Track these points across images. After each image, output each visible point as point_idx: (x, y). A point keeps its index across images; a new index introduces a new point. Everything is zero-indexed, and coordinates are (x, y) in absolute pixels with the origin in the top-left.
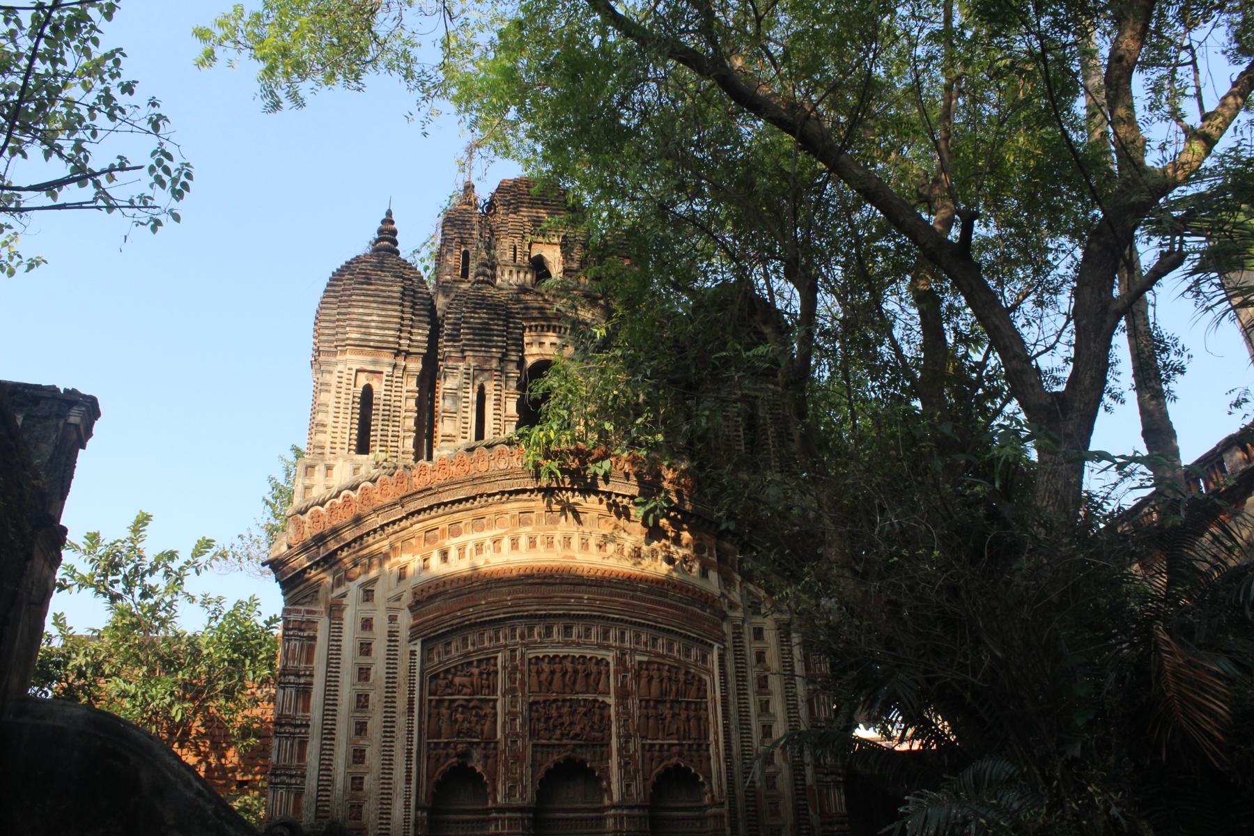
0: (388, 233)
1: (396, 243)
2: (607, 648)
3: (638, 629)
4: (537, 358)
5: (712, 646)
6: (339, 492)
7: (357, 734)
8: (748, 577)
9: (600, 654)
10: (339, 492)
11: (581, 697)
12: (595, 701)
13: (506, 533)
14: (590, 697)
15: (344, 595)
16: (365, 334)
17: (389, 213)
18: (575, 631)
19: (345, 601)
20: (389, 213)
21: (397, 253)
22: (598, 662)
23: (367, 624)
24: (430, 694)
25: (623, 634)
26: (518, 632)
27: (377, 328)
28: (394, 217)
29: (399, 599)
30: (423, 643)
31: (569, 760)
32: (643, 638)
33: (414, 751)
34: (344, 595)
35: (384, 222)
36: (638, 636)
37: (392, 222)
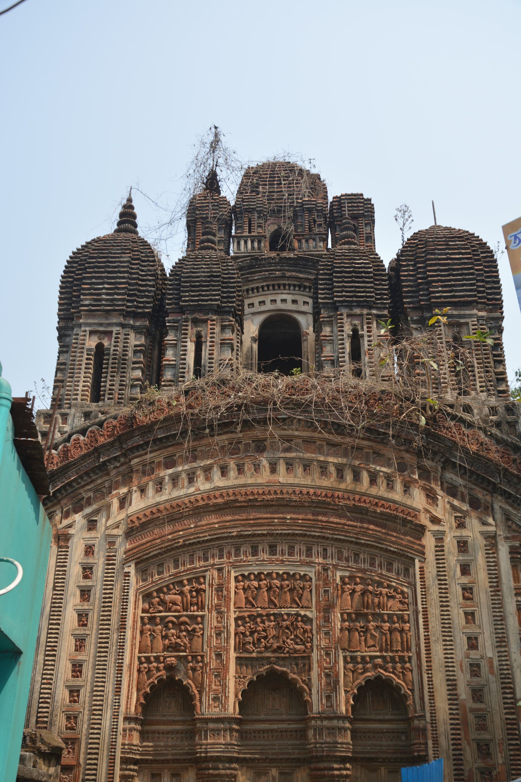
0: (128, 217)
1: (136, 226)
2: (309, 564)
3: (339, 544)
4: (269, 314)
5: (413, 560)
6: (70, 436)
7: (76, 650)
8: (452, 491)
9: (302, 571)
10: (70, 436)
11: (284, 611)
12: (298, 615)
13: (215, 463)
14: (293, 611)
15: (70, 526)
16: (96, 300)
17: (130, 200)
18: (279, 549)
19: (71, 531)
20: (130, 200)
21: (136, 233)
22: (303, 578)
23: (89, 550)
24: (143, 612)
25: (325, 550)
26: (377, 563)
27: (107, 294)
28: (134, 204)
29: (118, 527)
30: (136, 564)
31: (272, 672)
32: (345, 554)
33: (422, 630)
34: (70, 526)
35: (124, 207)
36: (340, 552)
37: (132, 207)
